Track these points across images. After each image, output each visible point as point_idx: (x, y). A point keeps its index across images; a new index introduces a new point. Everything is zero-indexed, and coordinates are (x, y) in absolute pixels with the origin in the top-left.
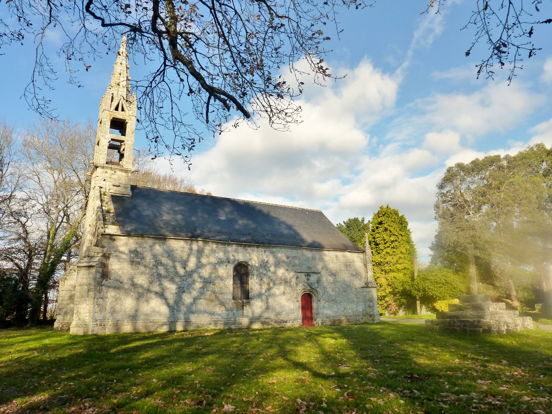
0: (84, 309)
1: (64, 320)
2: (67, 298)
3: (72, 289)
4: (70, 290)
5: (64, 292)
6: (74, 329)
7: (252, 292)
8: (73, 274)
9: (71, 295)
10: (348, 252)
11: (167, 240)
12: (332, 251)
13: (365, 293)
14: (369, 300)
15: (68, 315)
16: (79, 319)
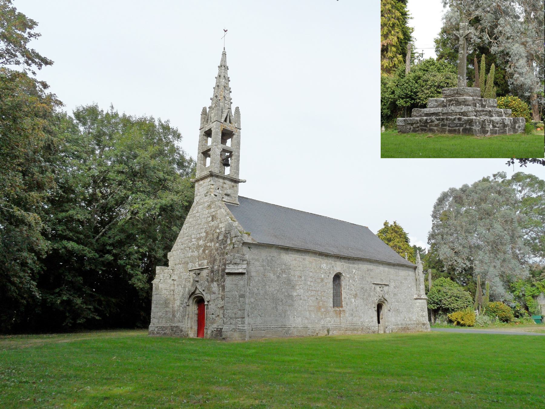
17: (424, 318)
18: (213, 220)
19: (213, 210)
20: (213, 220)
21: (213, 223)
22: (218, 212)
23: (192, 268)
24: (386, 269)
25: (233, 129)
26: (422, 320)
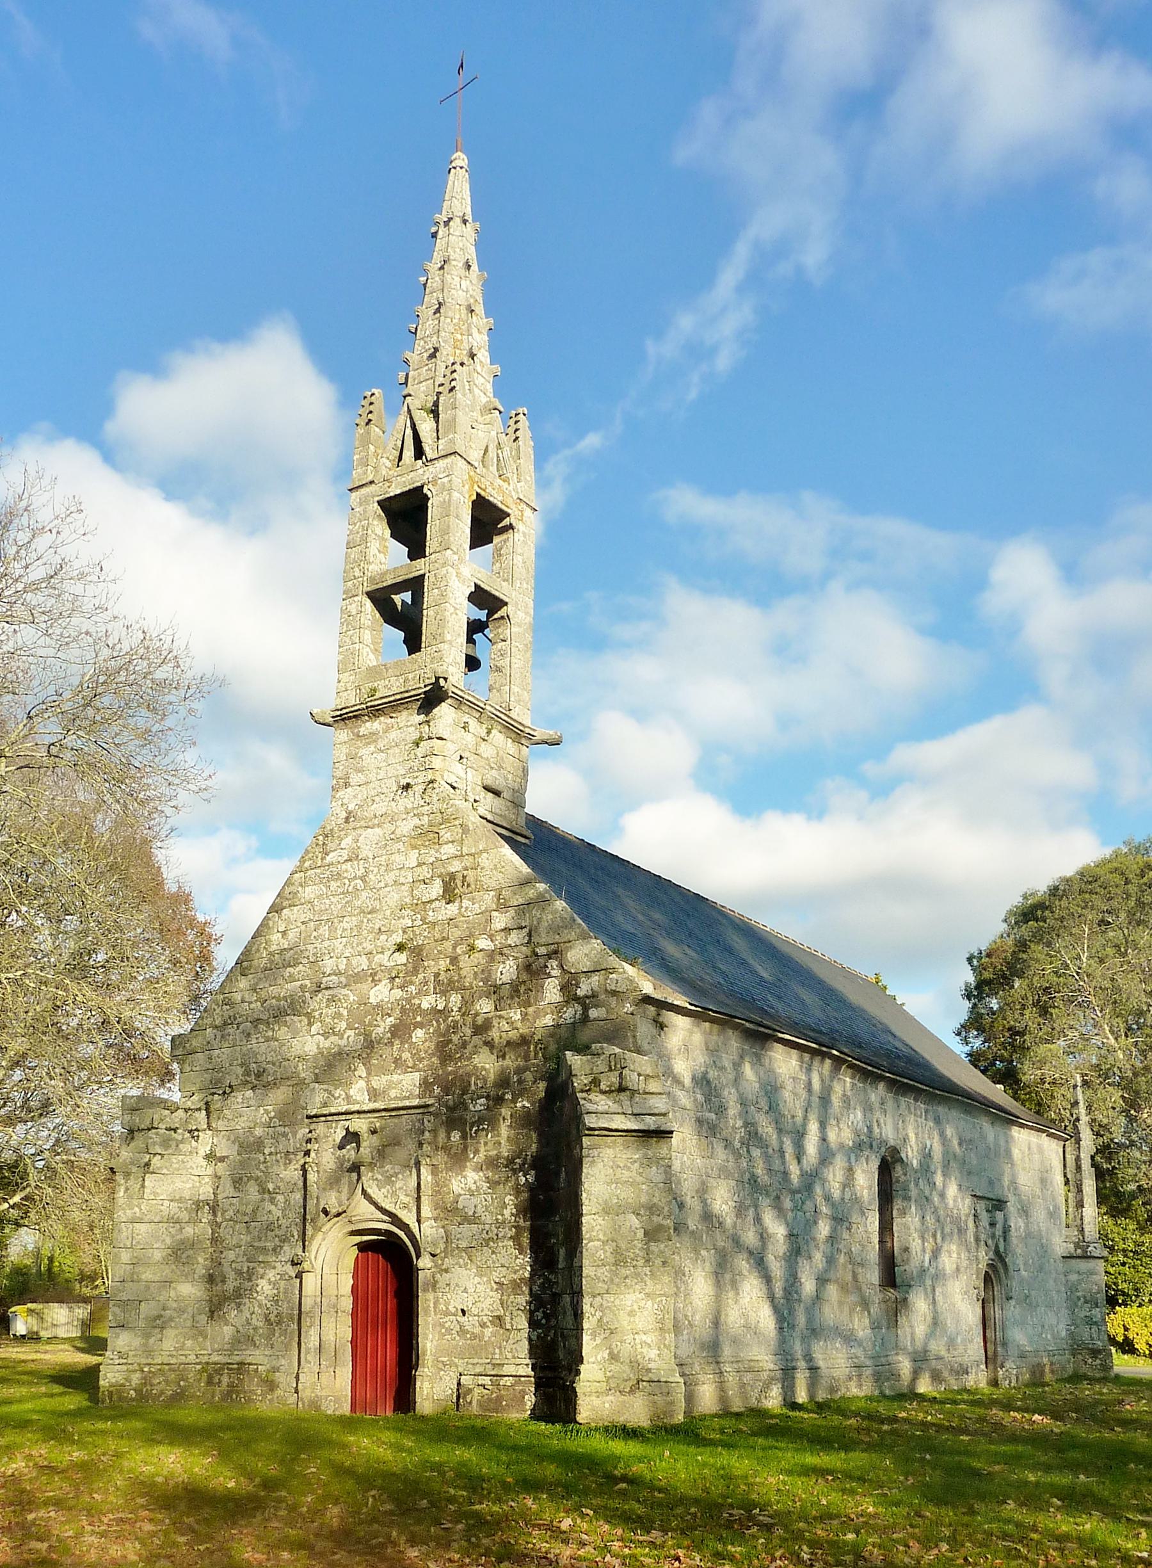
0: (631, 1313)
1: (148, 1352)
2: (158, 1255)
3: (185, 1216)
4: (175, 1221)
5: (142, 1228)
6: (596, 1402)
7: (906, 1261)
8: (184, 1147)
9: (182, 1242)
10: (1050, 1135)
11: (769, 1044)
12: (1031, 1128)
13: (1074, 1277)
14: (1086, 1302)
15: (170, 1333)
16: (614, 1357)
17: (1094, 1328)
18: (449, 895)
19: (449, 850)
20: (449, 895)
21: (453, 909)
22: (484, 860)
23: (325, 1105)
24: (620, 1128)
25: (509, 502)
26: (1086, 1337)
